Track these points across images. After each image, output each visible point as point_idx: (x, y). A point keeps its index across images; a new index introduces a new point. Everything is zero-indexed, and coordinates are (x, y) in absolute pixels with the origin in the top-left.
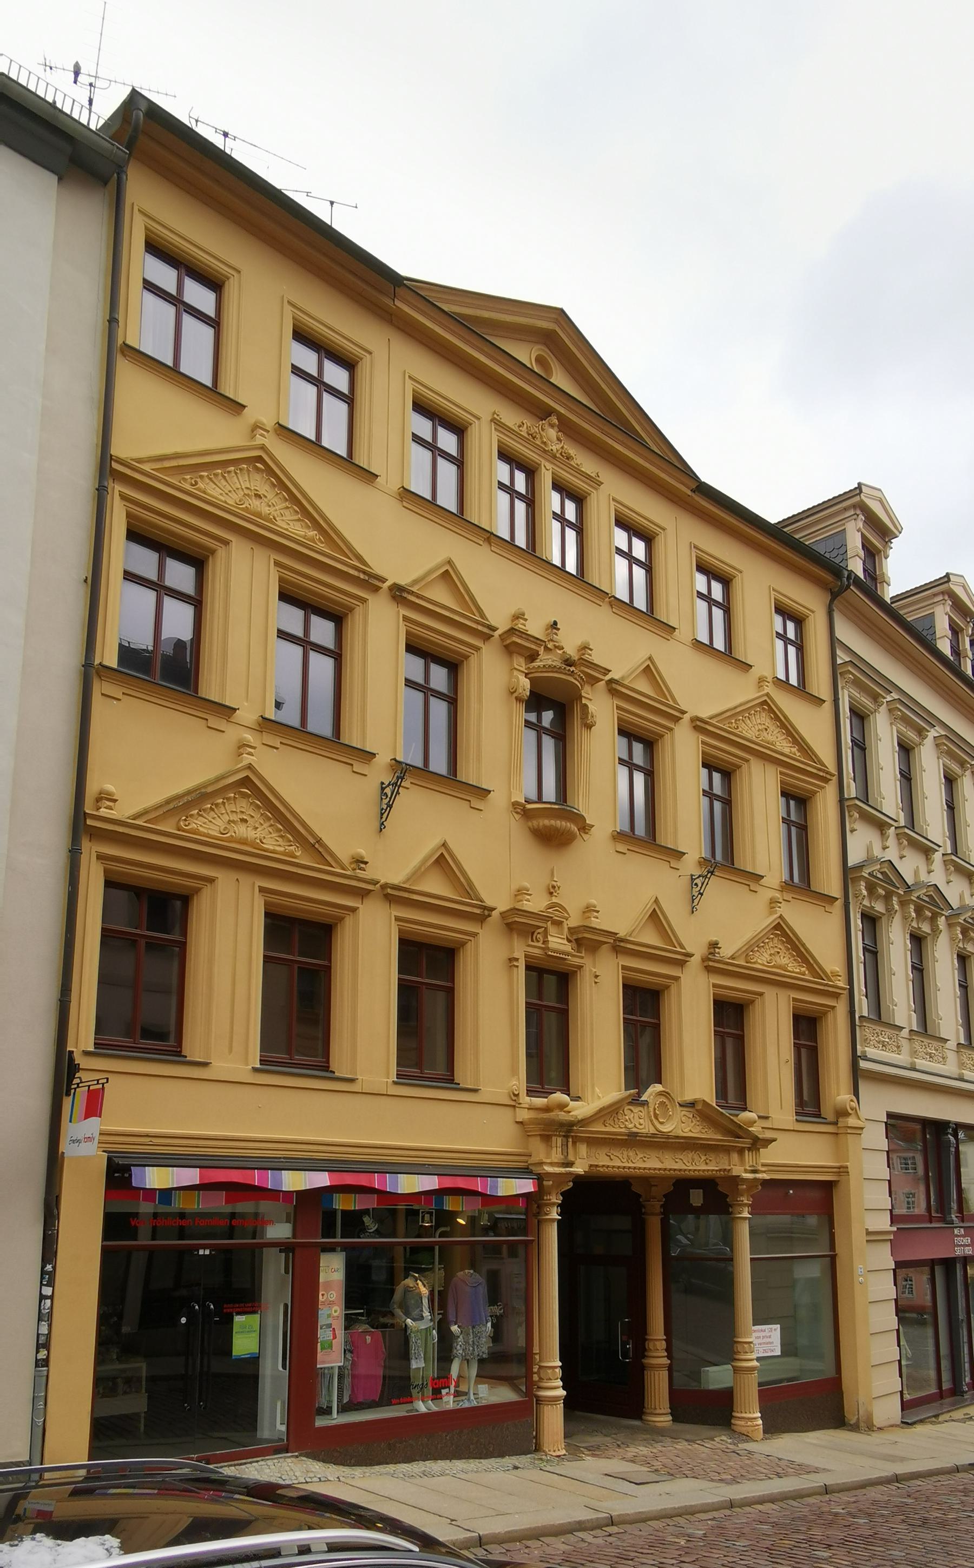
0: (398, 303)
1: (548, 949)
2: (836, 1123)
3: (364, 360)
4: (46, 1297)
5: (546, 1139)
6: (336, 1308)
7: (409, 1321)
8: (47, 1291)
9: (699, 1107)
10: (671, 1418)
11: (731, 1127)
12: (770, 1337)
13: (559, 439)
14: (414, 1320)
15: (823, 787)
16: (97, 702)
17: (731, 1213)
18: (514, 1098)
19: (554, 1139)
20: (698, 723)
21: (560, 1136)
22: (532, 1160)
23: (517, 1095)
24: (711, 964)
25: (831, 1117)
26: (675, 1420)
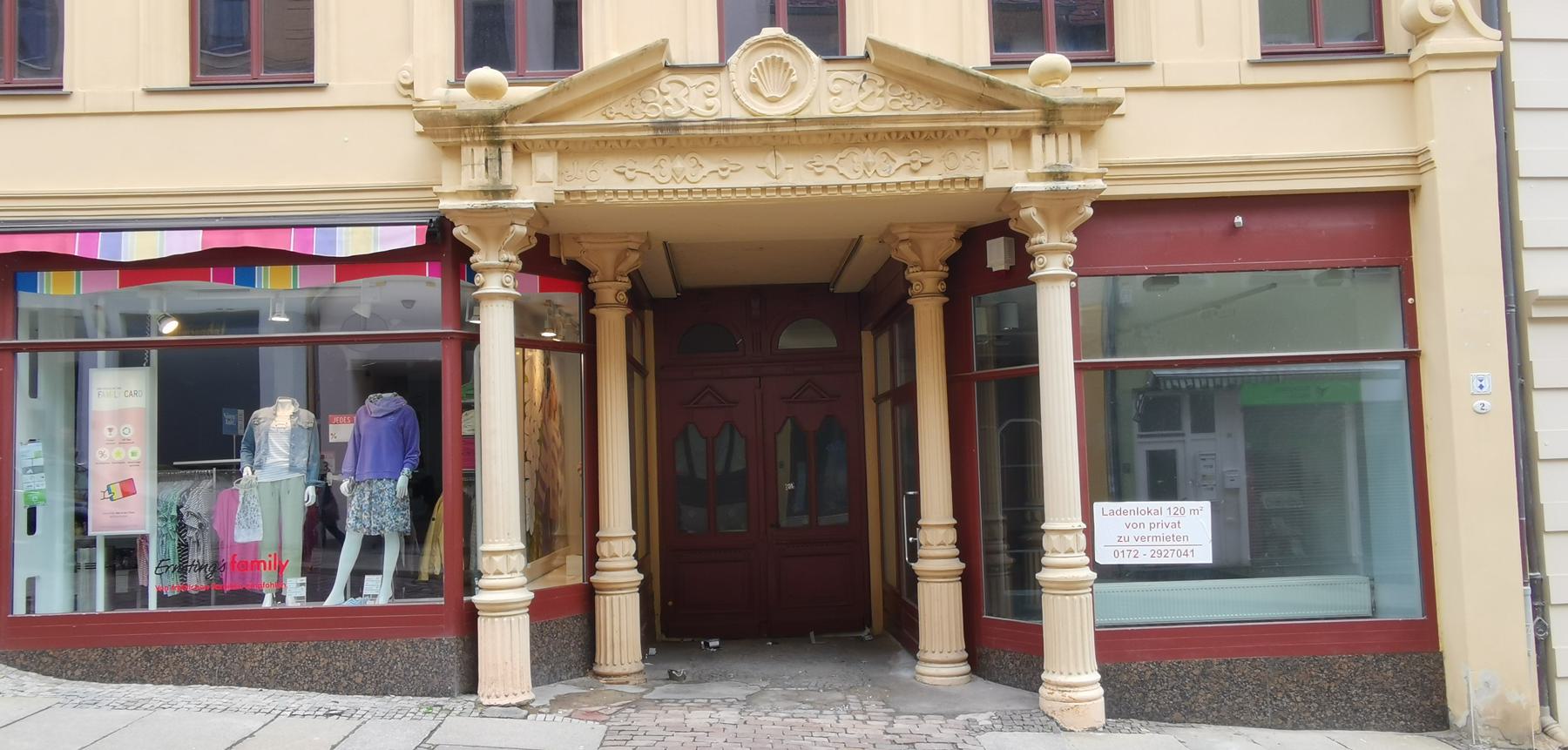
5: (453, 151)
6: (133, 448)
11: (976, 89)
12: (1176, 525)
18: (409, 92)
19: (465, 151)
21: (480, 143)
23: (411, 86)
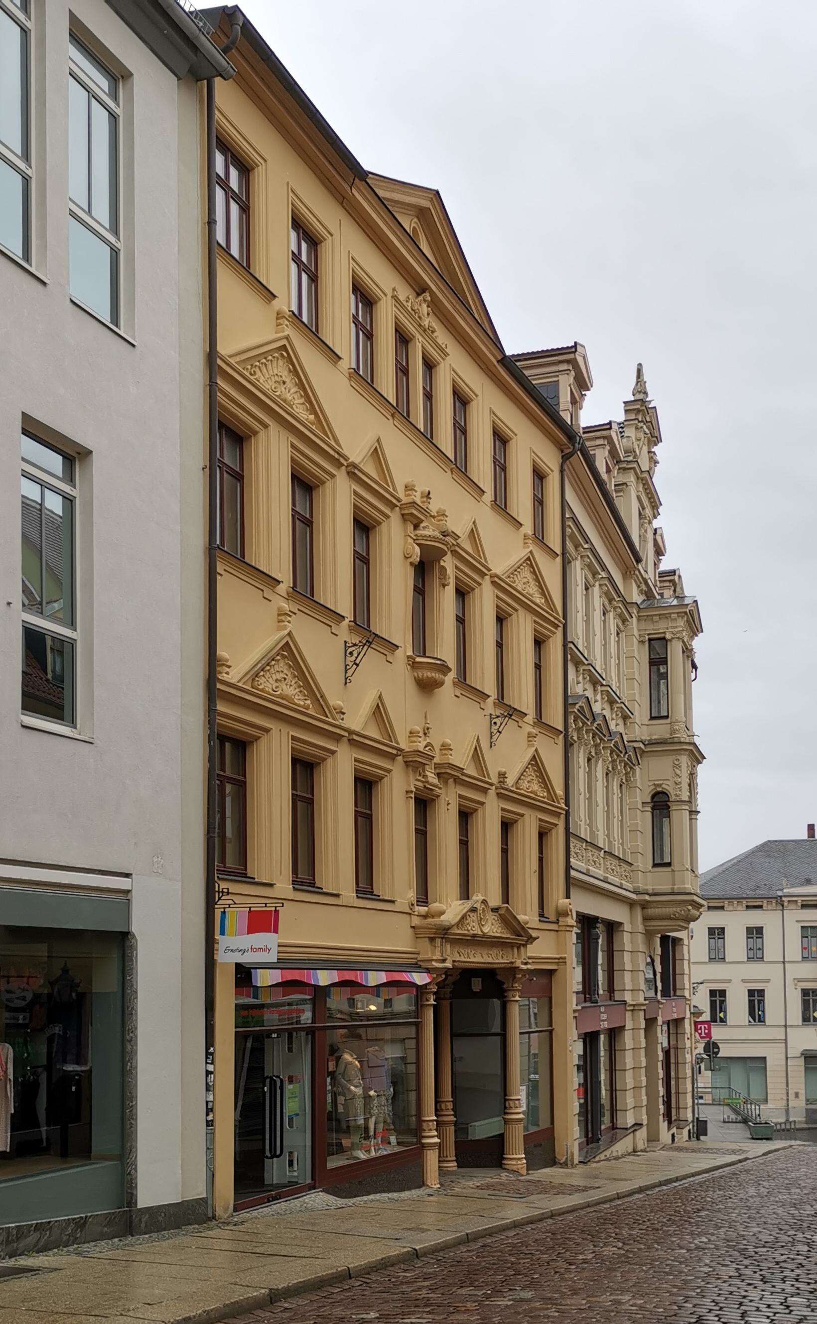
0: (354, 191)
1: (427, 782)
2: (557, 922)
3: (327, 242)
4: (212, 1073)
7: (352, 1088)
8: (210, 1068)
9: (502, 912)
10: (456, 1164)
13: (428, 314)
14: (356, 1087)
15: (555, 633)
16: (222, 583)
17: (506, 997)
20: (496, 579)
22: (420, 957)
24: (502, 791)
25: (553, 919)
26: (458, 1167)
